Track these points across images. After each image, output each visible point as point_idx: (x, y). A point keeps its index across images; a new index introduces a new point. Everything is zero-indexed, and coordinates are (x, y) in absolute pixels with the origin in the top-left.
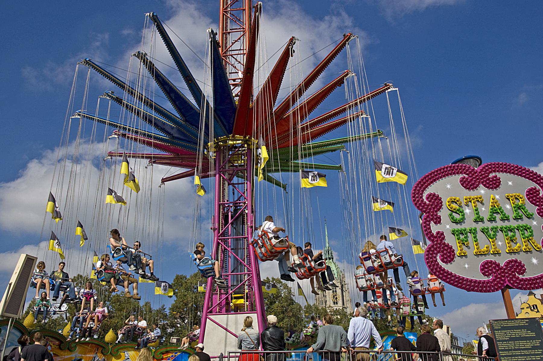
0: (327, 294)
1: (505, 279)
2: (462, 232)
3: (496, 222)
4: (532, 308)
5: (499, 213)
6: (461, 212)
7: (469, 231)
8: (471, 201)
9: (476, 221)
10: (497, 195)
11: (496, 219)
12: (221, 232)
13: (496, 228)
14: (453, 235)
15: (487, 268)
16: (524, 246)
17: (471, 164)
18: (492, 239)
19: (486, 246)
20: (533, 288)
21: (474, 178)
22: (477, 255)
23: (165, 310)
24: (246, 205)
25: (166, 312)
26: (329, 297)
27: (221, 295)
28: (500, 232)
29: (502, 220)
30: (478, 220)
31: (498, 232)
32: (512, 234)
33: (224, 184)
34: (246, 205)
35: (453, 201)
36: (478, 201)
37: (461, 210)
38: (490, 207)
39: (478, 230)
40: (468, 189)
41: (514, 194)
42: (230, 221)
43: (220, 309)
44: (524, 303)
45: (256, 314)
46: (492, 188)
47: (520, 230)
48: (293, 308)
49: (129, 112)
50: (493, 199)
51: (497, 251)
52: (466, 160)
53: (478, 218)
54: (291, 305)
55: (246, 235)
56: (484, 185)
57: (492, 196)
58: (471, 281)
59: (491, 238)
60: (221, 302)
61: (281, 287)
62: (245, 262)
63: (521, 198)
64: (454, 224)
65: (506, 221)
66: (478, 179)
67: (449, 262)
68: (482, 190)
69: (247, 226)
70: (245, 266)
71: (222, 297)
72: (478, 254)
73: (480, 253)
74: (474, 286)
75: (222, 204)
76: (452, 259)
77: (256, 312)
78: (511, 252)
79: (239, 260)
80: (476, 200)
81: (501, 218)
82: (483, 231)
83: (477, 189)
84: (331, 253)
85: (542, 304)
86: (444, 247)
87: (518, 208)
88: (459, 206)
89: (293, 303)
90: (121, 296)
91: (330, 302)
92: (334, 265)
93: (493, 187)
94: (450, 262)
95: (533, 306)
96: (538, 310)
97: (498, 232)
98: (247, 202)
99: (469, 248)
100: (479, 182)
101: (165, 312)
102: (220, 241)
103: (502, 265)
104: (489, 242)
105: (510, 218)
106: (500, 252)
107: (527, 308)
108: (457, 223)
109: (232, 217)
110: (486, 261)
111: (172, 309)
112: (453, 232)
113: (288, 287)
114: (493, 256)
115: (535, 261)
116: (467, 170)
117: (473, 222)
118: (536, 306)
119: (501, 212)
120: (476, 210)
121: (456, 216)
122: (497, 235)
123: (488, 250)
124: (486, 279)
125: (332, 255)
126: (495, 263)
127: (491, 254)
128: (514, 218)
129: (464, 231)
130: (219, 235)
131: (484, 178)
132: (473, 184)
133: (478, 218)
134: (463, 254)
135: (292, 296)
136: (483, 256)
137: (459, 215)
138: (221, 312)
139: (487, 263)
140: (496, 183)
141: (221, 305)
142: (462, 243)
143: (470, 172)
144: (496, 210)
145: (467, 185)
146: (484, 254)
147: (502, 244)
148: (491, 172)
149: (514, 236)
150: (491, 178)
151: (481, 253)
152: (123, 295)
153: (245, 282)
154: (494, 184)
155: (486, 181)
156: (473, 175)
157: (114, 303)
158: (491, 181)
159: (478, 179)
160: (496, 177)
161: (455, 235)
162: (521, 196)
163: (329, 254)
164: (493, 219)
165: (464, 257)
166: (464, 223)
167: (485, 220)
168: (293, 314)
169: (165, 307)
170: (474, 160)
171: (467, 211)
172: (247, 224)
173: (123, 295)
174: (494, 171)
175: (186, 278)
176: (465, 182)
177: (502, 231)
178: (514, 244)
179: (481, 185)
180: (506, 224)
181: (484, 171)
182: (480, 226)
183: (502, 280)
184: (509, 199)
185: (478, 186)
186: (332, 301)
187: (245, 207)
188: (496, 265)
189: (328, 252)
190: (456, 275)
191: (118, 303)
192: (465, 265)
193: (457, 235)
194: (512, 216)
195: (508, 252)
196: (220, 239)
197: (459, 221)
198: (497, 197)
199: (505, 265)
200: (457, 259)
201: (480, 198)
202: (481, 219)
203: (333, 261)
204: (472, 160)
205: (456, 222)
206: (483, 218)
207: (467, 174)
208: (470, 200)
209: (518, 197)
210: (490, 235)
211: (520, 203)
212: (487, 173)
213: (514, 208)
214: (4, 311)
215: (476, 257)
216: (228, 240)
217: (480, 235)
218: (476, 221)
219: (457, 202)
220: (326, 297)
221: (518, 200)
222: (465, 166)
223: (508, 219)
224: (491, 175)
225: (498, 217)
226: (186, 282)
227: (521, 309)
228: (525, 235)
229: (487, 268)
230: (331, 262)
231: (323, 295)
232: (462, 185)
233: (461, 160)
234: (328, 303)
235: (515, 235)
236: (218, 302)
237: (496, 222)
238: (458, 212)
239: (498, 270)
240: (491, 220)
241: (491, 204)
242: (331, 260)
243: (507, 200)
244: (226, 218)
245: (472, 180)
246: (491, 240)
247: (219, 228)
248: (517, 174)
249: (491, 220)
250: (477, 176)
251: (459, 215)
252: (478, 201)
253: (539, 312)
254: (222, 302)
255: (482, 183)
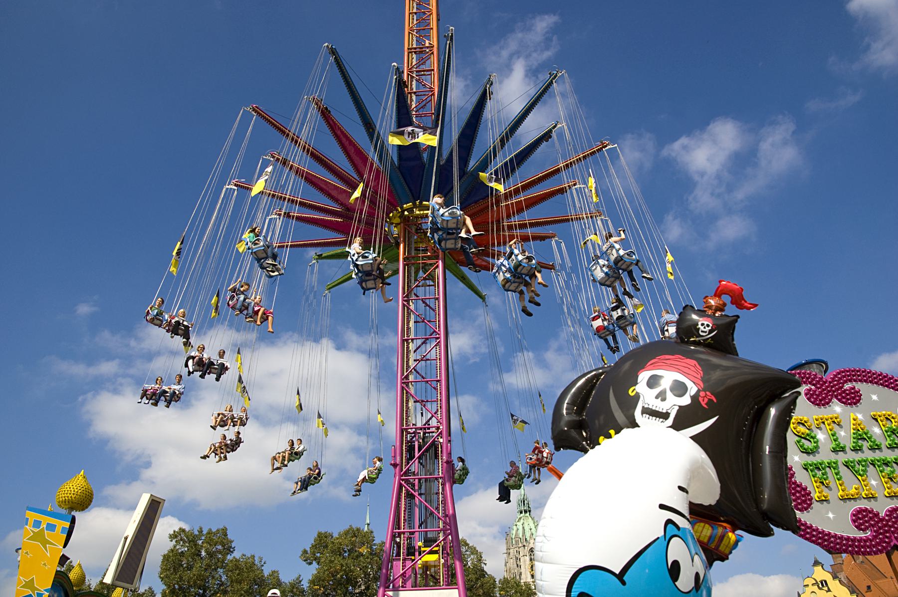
0: (521, 564)
1: (891, 536)
2: (817, 466)
3: (863, 452)
4: (820, 586)
5: (865, 439)
6: (812, 437)
7: (828, 465)
8: (823, 423)
9: (835, 451)
10: (857, 415)
11: (846, 448)
12: (404, 470)
13: (865, 461)
14: (805, 471)
15: (861, 518)
16: (817, 493)
17: (815, 370)
18: (861, 476)
19: (854, 486)
20: (869, 554)
21: (824, 390)
22: (843, 499)
23: (302, 583)
24: (440, 431)
25: (303, 585)
26: (525, 568)
27: (405, 561)
28: (871, 466)
29: (872, 449)
30: (839, 449)
31: (869, 467)
32: (889, 469)
33: (407, 401)
34: (440, 431)
35: (799, 423)
36: (834, 422)
37: (813, 435)
38: (852, 431)
39: (840, 464)
40: (818, 405)
41: (884, 412)
42: (417, 455)
43: (404, 582)
44: (808, 577)
45: (457, 590)
46: (850, 404)
47: (832, 468)
48: (485, 583)
49: (603, 287)
50: (854, 420)
51: (871, 494)
52: (806, 366)
53: (838, 446)
54: (482, 579)
55: (440, 473)
56: (840, 400)
57: (852, 416)
58: (841, 538)
59: (860, 475)
60: (405, 573)
61: (466, 551)
62: (439, 513)
63: (893, 418)
64: (805, 455)
65: (877, 451)
66: (829, 391)
67: (806, 510)
68: (837, 408)
69: (442, 462)
70: (439, 518)
71: (407, 565)
72: (845, 499)
73: (847, 496)
74: (847, 546)
75: (405, 429)
76: (810, 505)
77: (457, 587)
78: (893, 496)
79: (429, 508)
80: (821, 421)
81: (870, 446)
82: (846, 465)
83: (830, 406)
84: (528, 504)
85: (833, 579)
86: (796, 488)
87: (892, 432)
88: (808, 429)
89: (484, 575)
90: (241, 560)
91: (526, 575)
92: (532, 522)
93: (852, 402)
94: (806, 509)
95: (822, 582)
96: (828, 588)
97: (869, 467)
98: (441, 427)
99: (831, 489)
100: (832, 395)
101: (302, 587)
102: (403, 483)
103: (882, 514)
104: (858, 481)
105: (883, 447)
106: (877, 495)
107: (813, 584)
108: (808, 453)
109: (420, 449)
110: (859, 508)
111: (312, 582)
112: (805, 465)
113: (477, 551)
114: (866, 500)
115: (831, 515)
116: (813, 379)
117: (831, 452)
118: (825, 581)
119: (869, 438)
120: (833, 435)
121: (807, 444)
122: (867, 471)
123: (859, 493)
124: (861, 535)
125: (529, 506)
126: (871, 512)
127: (864, 498)
128: (853, 449)
129: (821, 464)
130: (402, 473)
131: (838, 389)
132: (824, 399)
133: (838, 445)
134: (824, 499)
135: (483, 565)
136: (852, 501)
137: (810, 441)
138: (405, 587)
139: (860, 511)
140: (855, 396)
141: (405, 576)
142: (820, 482)
143: (818, 382)
144: (861, 436)
145: (816, 399)
146: (853, 499)
147: (877, 484)
148: (846, 382)
149: (892, 472)
150: (847, 390)
151: (848, 497)
152: (243, 559)
153: (440, 542)
154: (852, 399)
155: (840, 394)
156: (822, 385)
157: (231, 571)
158: (848, 395)
159: (829, 391)
160: (854, 388)
161: (809, 470)
162: (893, 415)
163: (524, 504)
164: (858, 448)
165: (825, 503)
166: (819, 453)
167: (847, 449)
168: (484, 592)
169: (300, 579)
170: (818, 365)
171: (821, 436)
172: (441, 459)
173: (243, 559)
174: (850, 381)
175: (332, 537)
176: (812, 395)
177: (874, 465)
178: (894, 484)
179: (835, 400)
180: (877, 455)
181: (836, 381)
182: (842, 458)
183: (887, 537)
184: (876, 420)
185: (830, 400)
186: (529, 573)
187: (439, 434)
188: (874, 514)
189: (524, 501)
190: (824, 531)
191: (237, 572)
192: (827, 513)
193: (812, 471)
194: (849, 444)
195: (887, 495)
196: (403, 480)
197: (811, 450)
198: (860, 416)
199: (887, 515)
200: (815, 505)
201: (836, 418)
202: (841, 447)
203: (530, 514)
204: (814, 365)
205: (807, 452)
206: (845, 447)
207: (813, 385)
208: (823, 421)
209: (889, 417)
210: (859, 471)
211: (893, 425)
212: (841, 383)
213: (887, 432)
214: (115, 578)
215: (842, 502)
216: (415, 481)
217: (843, 470)
218: (835, 451)
219: (805, 424)
220: (520, 567)
221: (889, 421)
222: (810, 374)
223: (879, 449)
224: (847, 386)
225: (866, 445)
226: (333, 543)
227: (804, 586)
228: (839, 475)
229: (861, 518)
230: (527, 517)
231: (515, 565)
232: (808, 399)
233: (800, 366)
234: (523, 576)
235: (894, 470)
236: (402, 572)
237: (863, 452)
238: (808, 438)
239: (878, 522)
240: (857, 449)
241: (852, 426)
242: (528, 514)
243: (874, 421)
244: (411, 449)
245: (821, 392)
246: (859, 477)
247: (402, 463)
248: (881, 384)
249: (857, 449)
250: (827, 387)
251: (810, 441)
252: (834, 422)
253: (830, 591)
254: (407, 572)
255: (836, 397)
